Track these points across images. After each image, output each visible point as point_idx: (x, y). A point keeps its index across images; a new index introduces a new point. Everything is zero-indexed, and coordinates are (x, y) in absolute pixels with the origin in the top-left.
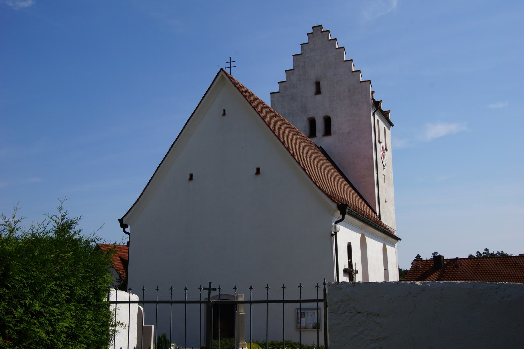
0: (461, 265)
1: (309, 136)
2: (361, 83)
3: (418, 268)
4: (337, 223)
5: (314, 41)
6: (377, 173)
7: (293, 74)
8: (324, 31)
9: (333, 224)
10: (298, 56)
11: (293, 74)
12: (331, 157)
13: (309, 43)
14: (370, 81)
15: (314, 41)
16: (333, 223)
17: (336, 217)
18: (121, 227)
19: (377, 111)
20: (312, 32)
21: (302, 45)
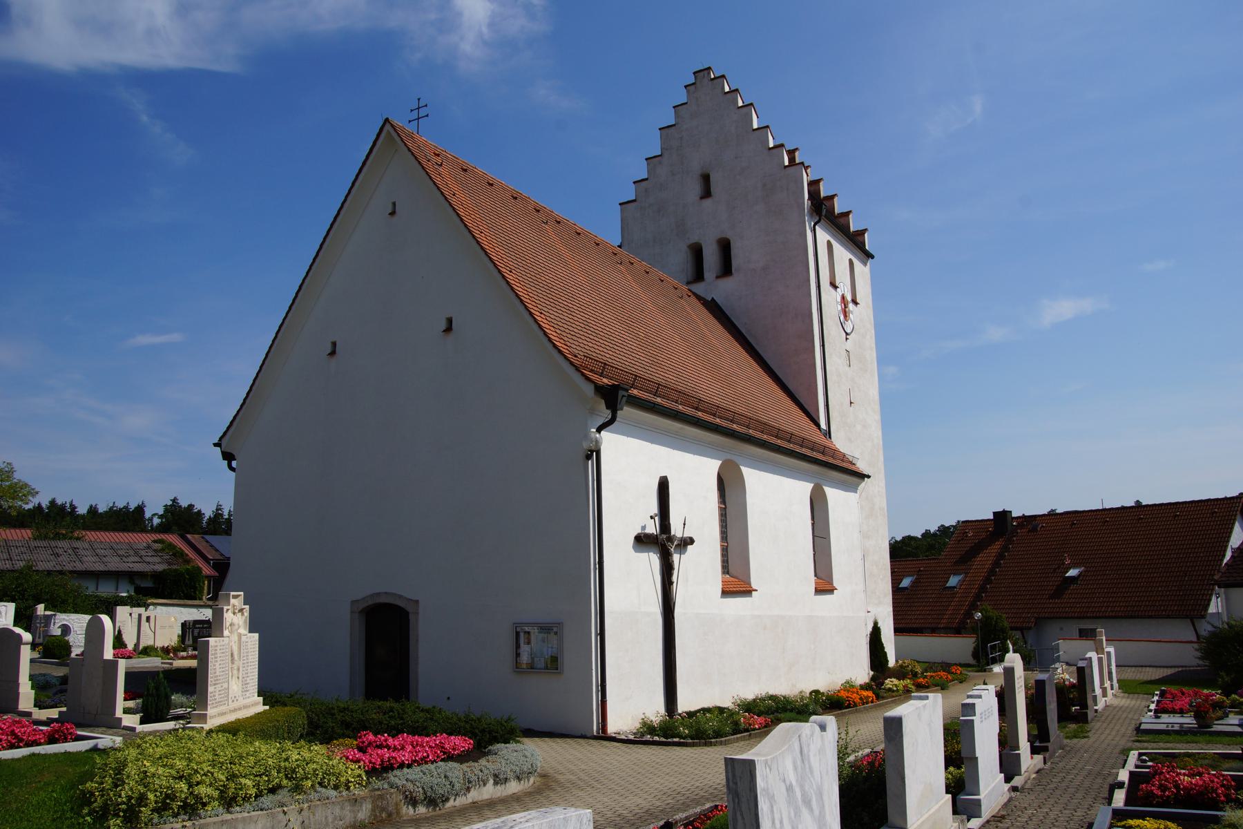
0: (1042, 526)
1: (690, 279)
3: (967, 536)
4: (599, 430)
10: (670, 128)
11: (660, 163)
12: (733, 319)
19: (822, 220)
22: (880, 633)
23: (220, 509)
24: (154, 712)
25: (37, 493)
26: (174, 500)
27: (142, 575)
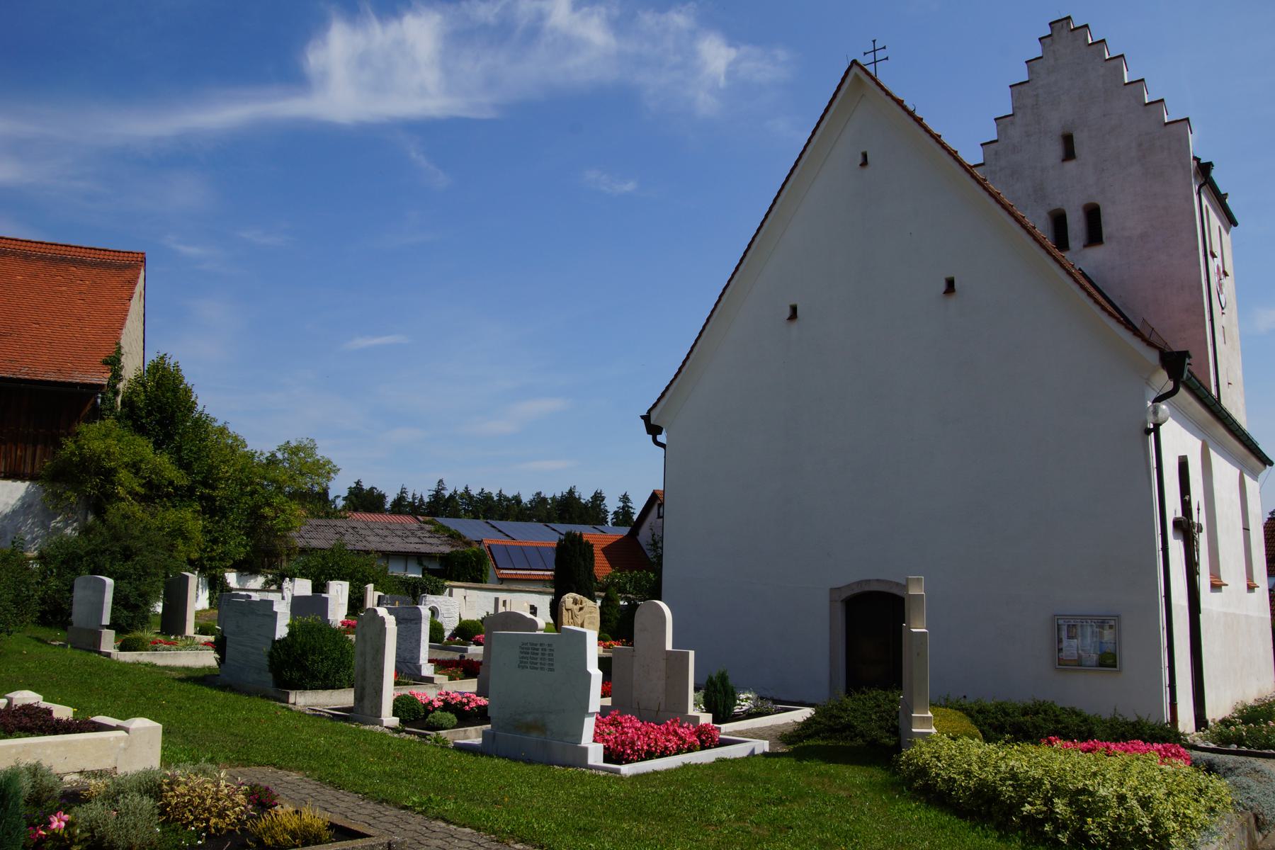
2: (1168, 126)
4: (1159, 399)
5: (1054, 51)
6: (1212, 320)
7: (1012, 123)
8: (1075, 29)
9: (1149, 404)
10: (1022, 85)
11: (1012, 123)
13: (1044, 58)
14: (1187, 119)
15: (1054, 51)
16: (1148, 402)
17: (1154, 387)
18: (648, 433)
20: (1050, 33)
21: (1029, 63)
22: (551, 611)
23: (405, 492)
24: (722, 710)
25: (339, 470)
26: (358, 483)
27: (430, 556)
